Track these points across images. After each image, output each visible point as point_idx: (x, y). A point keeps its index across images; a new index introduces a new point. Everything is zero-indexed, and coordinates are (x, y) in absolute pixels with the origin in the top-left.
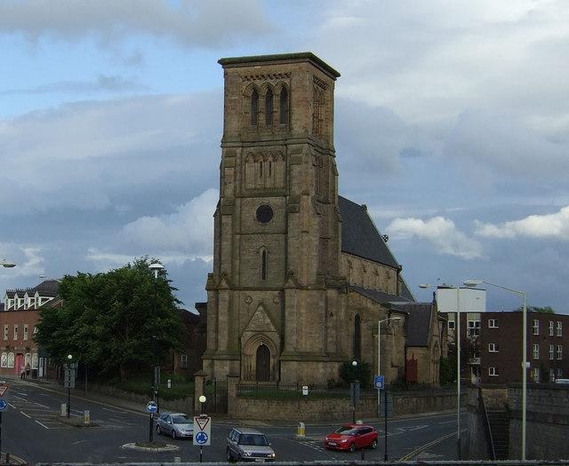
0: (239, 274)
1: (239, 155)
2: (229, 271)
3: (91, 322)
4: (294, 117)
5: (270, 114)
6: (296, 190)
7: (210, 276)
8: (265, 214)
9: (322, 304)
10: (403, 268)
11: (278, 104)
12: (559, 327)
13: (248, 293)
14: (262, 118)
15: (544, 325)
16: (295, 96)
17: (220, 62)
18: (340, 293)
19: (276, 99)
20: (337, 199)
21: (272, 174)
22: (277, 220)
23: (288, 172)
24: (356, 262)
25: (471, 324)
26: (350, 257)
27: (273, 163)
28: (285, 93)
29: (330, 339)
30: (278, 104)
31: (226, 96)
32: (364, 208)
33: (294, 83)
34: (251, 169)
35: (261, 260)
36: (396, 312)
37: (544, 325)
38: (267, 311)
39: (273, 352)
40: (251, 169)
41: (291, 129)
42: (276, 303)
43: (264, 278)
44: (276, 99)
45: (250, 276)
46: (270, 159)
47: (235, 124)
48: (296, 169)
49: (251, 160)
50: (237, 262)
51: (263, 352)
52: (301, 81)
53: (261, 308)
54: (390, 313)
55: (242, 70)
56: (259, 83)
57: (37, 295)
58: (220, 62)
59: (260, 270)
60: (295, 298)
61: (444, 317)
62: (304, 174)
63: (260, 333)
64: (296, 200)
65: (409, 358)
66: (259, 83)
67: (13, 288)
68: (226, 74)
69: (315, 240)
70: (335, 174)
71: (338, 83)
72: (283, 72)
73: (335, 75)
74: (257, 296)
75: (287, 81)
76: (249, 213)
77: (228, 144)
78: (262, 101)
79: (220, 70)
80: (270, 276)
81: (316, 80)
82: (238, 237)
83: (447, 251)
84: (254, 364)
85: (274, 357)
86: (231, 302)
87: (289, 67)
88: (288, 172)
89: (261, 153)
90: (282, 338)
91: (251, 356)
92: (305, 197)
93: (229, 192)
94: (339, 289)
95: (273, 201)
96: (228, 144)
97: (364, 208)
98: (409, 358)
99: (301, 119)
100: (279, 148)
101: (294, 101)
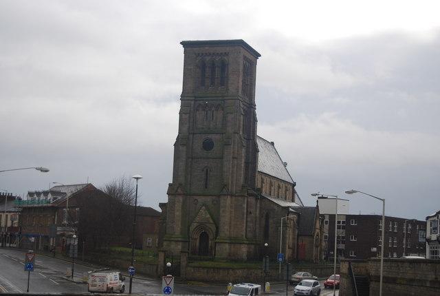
6: (230, 130)
8: (208, 145)
11: (218, 77)
13: (195, 197)
28: (224, 66)
30: (218, 77)
40: (200, 115)
41: (227, 89)
49: (201, 109)
51: (204, 237)
67: (33, 190)
74: (201, 199)
79: (182, 49)
84: (198, 244)
86: (184, 202)
90: (217, 228)
93: (185, 129)
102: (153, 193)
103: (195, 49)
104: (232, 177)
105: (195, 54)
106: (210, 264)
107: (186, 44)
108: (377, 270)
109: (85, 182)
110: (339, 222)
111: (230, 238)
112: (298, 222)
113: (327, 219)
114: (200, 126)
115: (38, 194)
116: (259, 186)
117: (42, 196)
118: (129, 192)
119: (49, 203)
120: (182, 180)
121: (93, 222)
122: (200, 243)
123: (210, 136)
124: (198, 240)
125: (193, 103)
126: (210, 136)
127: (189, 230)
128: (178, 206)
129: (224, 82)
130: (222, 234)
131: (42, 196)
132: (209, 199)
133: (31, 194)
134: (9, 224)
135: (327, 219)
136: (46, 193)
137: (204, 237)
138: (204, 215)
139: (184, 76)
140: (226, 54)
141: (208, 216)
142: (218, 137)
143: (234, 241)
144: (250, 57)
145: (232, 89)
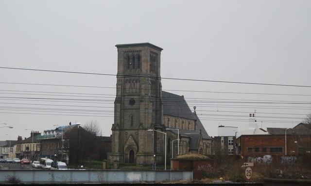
0: (123, 124)
2: (119, 123)
3: (216, 172)
4: (143, 66)
5: (134, 65)
6: (143, 93)
8: (132, 102)
10: (35, 130)
11: (138, 63)
13: (127, 131)
14: (131, 66)
16: (143, 59)
19: (136, 60)
20: (161, 93)
24: (172, 119)
28: (139, 57)
30: (138, 63)
32: (183, 96)
33: (142, 54)
34: (128, 86)
40: (128, 86)
41: (141, 71)
44: (136, 60)
47: (122, 69)
49: (128, 82)
50: (122, 120)
51: (132, 153)
52: (145, 56)
53: (188, 140)
55: (124, 49)
56: (130, 54)
57: (55, 132)
63: (130, 146)
64: (143, 97)
66: (130, 54)
67: (46, 130)
71: (162, 52)
72: (138, 50)
73: (161, 49)
74: (129, 132)
76: (127, 100)
79: (116, 49)
82: (123, 110)
83: (223, 114)
84: (128, 157)
86: (120, 135)
87: (141, 48)
88: (140, 86)
90: (138, 147)
93: (120, 94)
97: (183, 96)
99: (145, 67)
101: (142, 61)
102: (105, 129)
103: (123, 49)
104: (145, 122)
105: (123, 51)
106: (133, 167)
107: (119, 47)
108: (162, 152)
109: (64, 122)
110: (230, 141)
111: (145, 153)
112: (190, 142)
113: (222, 139)
114: (128, 92)
115: (49, 131)
116: (193, 112)
117: (48, 133)
118: (95, 133)
119: (54, 137)
120: (118, 122)
121: (78, 146)
122: (130, 156)
123: (132, 97)
124: (129, 155)
125: (123, 79)
126: (132, 97)
127: (123, 149)
128: (117, 137)
129: (139, 66)
130: (140, 151)
131: (48, 133)
132: (134, 132)
133: (45, 132)
134: (35, 150)
135: (222, 139)
136: (53, 131)
137: (132, 153)
138: (131, 141)
139: (118, 55)
140: (140, 51)
141: (133, 141)
142: (137, 97)
143: (147, 155)
144: (155, 51)
145: (144, 71)
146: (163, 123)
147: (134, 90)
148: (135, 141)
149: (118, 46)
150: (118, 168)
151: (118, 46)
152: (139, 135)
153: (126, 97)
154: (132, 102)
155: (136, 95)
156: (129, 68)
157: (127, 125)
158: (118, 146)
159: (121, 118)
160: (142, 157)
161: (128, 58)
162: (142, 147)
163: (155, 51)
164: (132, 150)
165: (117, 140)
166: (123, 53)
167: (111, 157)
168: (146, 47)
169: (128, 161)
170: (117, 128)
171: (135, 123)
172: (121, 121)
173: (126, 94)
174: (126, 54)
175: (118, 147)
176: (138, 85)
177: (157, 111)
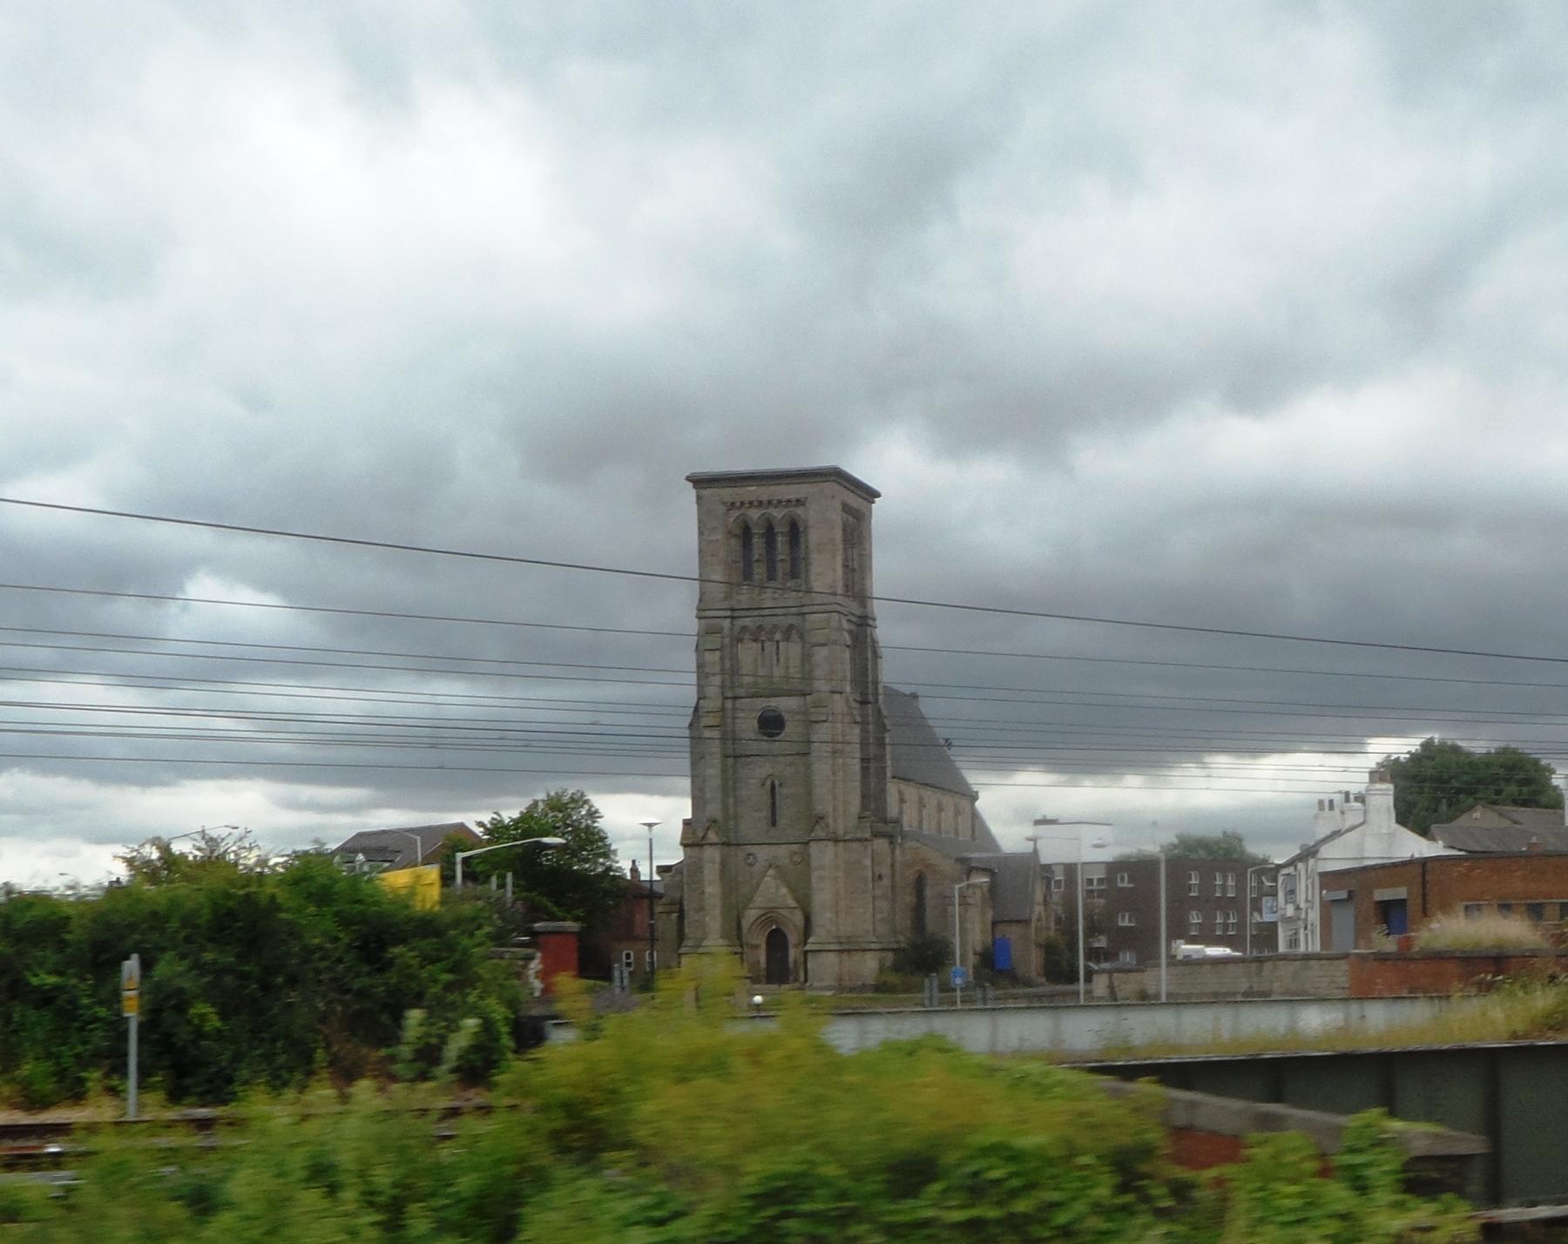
1: (726, 631)
2: (719, 815)
6: (822, 686)
7: (686, 823)
8: (771, 724)
9: (868, 862)
12: (1231, 883)
13: (750, 849)
14: (759, 571)
15: (1207, 879)
16: (814, 536)
17: (688, 479)
18: (1372, 773)
19: (781, 542)
21: (782, 660)
22: (791, 730)
23: (806, 658)
24: (911, 793)
25: (1090, 881)
26: (902, 786)
27: (782, 644)
28: (795, 531)
29: (879, 916)
31: (701, 533)
35: (767, 798)
36: (977, 869)
37: (1207, 879)
38: (782, 875)
39: (793, 938)
40: (747, 653)
42: (795, 864)
43: (774, 823)
44: (781, 542)
45: (752, 822)
46: (778, 636)
48: (821, 654)
50: (731, 800)
51: (777, 941)
54: (1325, 1173)
55: (728, 493)
56: (755, 514)
58: (688, 479)
59: (766, 813)
60: (823, 856)
61: (1047, 868)
62: (832, 663)
63: (768, 916)
65: (998, 936)
68: (699, 498)
69: (856, 766)
70: (876, 656)
72: (793, 497)
73: (878, 495)
74: (763, 854)
75: (800, 511)
77: (708, 613)
78: (758, 543)
79: (690, 493)
80: (782, 822)
81: (846, 508)
82: (731, 760)
84: (763, 959)
85: (796, 946)
86: (724, 865)
88: (806, 658)
89: (994, 923)
90: (808, 920)
91: (757, 947)
92: (837, 696)
94: (891, 838)
95: (784, 704)
96: (708, 613)
98: (998, 936)
99: (825, 572)
100: (791, 620)
101: (811, 546)
120: (713, 809)
122: (769, 957)
123: (774, 703)
126: (774, 703)
132: (782, 851)
141: (784, 890)
143: (848, 948)
144: (855, 501)
146: (892, 810)
147: (778, 672)
148: (793, 890)
149: (701, 482)
150: (940, 1004)
151: (701, 482)
152: (814, 863)
153: (739, 703)
154: (771, 724)
155: (789, 693)
156: (747, 575)
157: (752, 822)
158: (718, 912)
159: (725, 793)
160: (832, 957)
161: (745, 534)
162: (828, 915)
163: (855, 501)
164: (777, 930)
165: (712, 888)
166: (723, 509)
167: (535, 965)
168: (830, 487)
169: (764, 973)
170: (712, 836)
171: (786, 813)
172: (725, 807)
173: (741, 692)
174: (735, 513)
175: (719, 919)
176: (793, 650)
177: (871, 765)
